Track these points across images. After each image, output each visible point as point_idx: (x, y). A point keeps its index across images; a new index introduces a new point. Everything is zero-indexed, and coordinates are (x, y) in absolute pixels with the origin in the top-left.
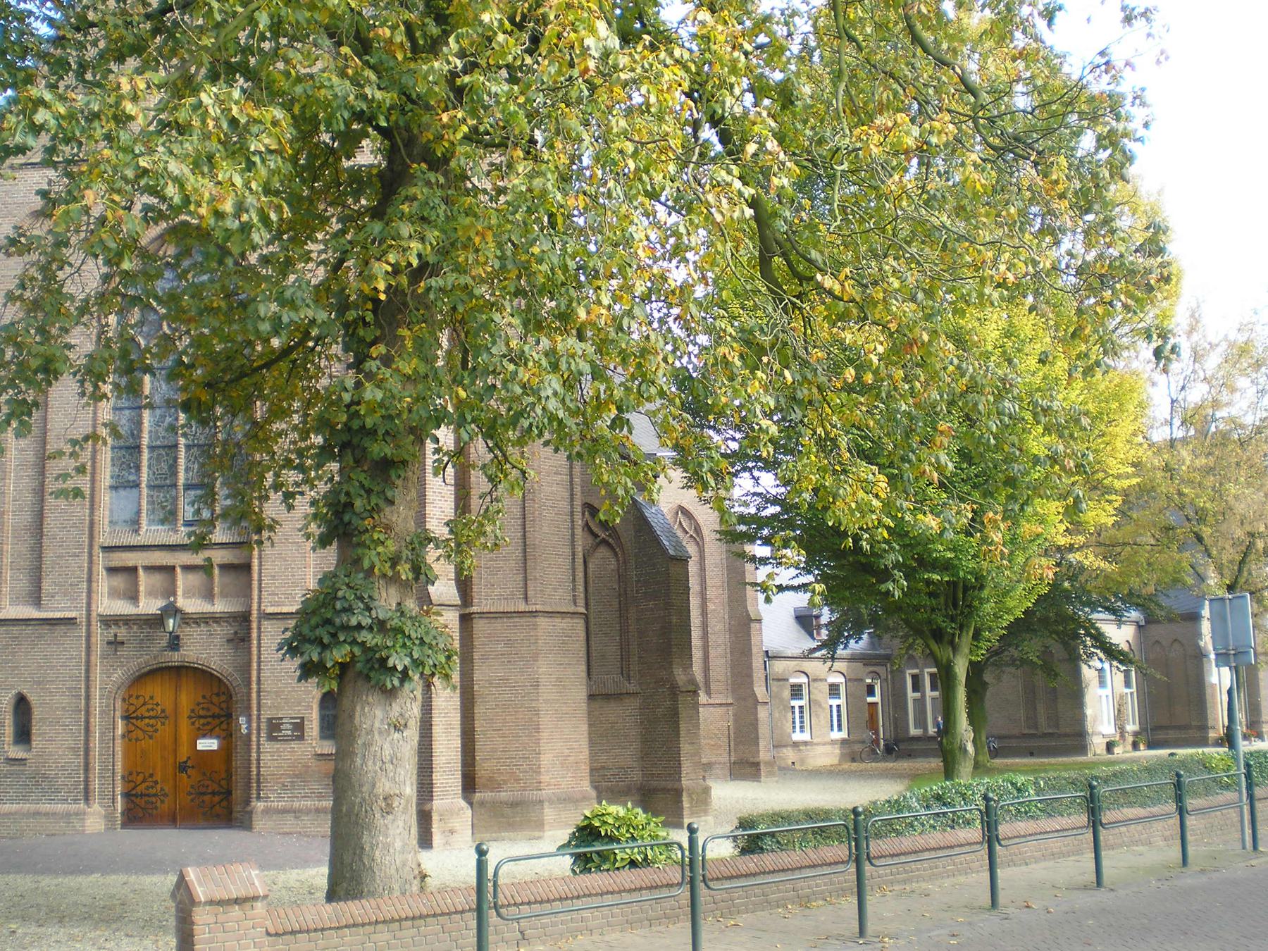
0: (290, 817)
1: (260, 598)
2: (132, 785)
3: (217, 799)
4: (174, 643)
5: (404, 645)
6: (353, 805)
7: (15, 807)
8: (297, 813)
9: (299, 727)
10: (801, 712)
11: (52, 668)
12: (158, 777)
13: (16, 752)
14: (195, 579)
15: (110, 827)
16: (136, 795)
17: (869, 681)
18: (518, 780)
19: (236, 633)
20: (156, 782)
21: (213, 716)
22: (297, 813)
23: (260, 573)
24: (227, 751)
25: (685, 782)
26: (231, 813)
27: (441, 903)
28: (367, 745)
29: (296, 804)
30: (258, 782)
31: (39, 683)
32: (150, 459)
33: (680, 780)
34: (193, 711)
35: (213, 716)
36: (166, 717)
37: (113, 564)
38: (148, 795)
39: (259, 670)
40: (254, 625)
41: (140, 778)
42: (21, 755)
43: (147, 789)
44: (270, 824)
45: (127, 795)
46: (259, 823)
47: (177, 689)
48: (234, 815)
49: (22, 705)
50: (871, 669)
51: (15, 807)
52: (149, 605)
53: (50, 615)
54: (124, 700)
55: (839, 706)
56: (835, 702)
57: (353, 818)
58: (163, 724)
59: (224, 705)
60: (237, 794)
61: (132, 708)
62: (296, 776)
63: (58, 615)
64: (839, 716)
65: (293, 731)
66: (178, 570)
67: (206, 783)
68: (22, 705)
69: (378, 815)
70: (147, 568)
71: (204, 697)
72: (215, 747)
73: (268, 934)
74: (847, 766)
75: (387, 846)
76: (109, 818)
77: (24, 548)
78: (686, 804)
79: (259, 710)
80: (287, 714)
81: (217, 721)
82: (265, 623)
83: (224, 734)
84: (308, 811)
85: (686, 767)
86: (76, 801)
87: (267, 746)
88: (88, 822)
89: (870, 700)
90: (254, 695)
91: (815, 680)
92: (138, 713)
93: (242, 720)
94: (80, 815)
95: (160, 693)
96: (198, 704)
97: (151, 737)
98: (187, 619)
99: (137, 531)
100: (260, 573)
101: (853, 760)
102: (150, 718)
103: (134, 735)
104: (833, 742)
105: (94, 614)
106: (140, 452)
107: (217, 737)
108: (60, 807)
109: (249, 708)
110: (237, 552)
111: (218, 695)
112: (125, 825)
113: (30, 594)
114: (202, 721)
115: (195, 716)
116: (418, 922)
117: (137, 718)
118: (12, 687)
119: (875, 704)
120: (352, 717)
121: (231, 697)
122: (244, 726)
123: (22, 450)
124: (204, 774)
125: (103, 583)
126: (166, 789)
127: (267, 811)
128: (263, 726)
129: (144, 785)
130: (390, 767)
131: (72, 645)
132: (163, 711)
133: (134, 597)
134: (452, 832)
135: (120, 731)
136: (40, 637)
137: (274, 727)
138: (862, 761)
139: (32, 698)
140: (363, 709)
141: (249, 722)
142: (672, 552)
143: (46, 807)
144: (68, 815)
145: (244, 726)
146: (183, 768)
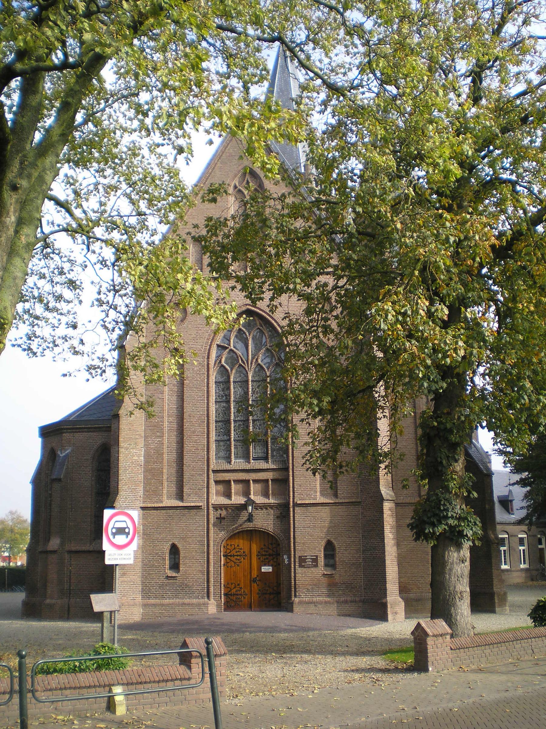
0: (312, 606)
1: (294, 496)
2: (229, 589)
3: (272, 596)
4: (250, 519)
5: (468, 525)
6: (446, 595)
7: (171, 601)
8: (315, 603)
9: (315, 560)
10: (505, 554)
11: (190, 531)
12: (242, 585)
13: (170, 573)
14: (259, 486)
15: (219, 611)
16: (231, 595)
17: (539, 536)
18: (419, 588)
19: (281, 513)
20: (241, 588)
21: (270, 555)
22: (315, 603)
23: (293, 484)
24: (277, 572)
25: (495, 589)
26: (280, 604)
27: (172, 672)
28: (451, 570)
29: (315, 599)
30: (295, 588)
31: (183, 538)
32: (234, 427)
33: (492, 588)
34: (259, 552)
35: (270, 555)
36: (245, 555)
37: (218, 479)
38: (237, 595)
39: (294, 532)
40: (291, 509)
41: (233, 586)
42: (174, 574)
43: (236, 591)
44: (302, 609)
45: (225, 595)
46: (296, 608)
47: (251, 540)
48: (282, 604)
49: (174, 550)
50: (540, 529)
51: (171, 601)
52: (238, 499)
53: (189, 504)
54: (224, 547)
55: (524, 550)
56: (521, 548)
57: (446, 602)
58: (244, 559)
59: (275, 550)
60: (284, 594)
61: (228, 551)
62: (315, 585)
63: (192, 504)
64: (524, 555)
65: (312, 562)
66: (251, 482)
67: (267, 588)
68: (174, 550)
69: (458, 600)
70: (234, 481)
71: (265, 545)
72: (271, 570)
73: (451, 649)
74: (530, 583)
75: (462, 615)
76: (218, 606)
77: (173, 471)
78: (496, 601)
79: (295, 552)
80: (309, 554)
81: (271, 557)
82: (296, 508)
83: (275, 564)
84: (321, 603)
85: (495, 582)
86: (203, 598)
87: (299, 570)
88: (210, 608)
89: (540, 546)
90: (292, 545)
91: (512, 536)
92: (232, 553)
93: (285, 557)
94: (206, 605)
95: (242, 544)
96: (262, 549)
97: (238, 565)
98: (257, 507)
99: (230, 462)
100: (293, 484)
101: (532, 580)
102: (237, 556)
103: (229, 565)
104: (522, 570)
105: (210, 504)
106: (230, 423)
107: (272, 566)
108: (195, 601)
109: (290, 550)
110: (275, 473)
111: (272, 544)
112: (225, 610)
113: (177, 494)
114: (264, 557)
115: (259, 555)
116: (499, 645)
117: (231, 556)
118: (170, 540)
119: (542, 549)
120: (443, 557)
121: (279, 545)
122: (286, 560)
123: (171, 422)
124: (266, 584)
125: (213, 488)
126: (246, 591)
127: (300, 603)
128: (297, 560)
129: (235, 590)
130: (461, 579)
131: (200, 519)
132: (244, 552)
133: (228, 495)
134: (396, 613)
135: (222, 563)
136: (184, 515)
137: (302, 561)
138: (537, 580)
139: (180, 546)
140: (449, 553)
141: (289, 558)
142: (485, 472)
143: (187, 601)
144: (199, 605)
145: (286, 560)
146: (254, 581)
